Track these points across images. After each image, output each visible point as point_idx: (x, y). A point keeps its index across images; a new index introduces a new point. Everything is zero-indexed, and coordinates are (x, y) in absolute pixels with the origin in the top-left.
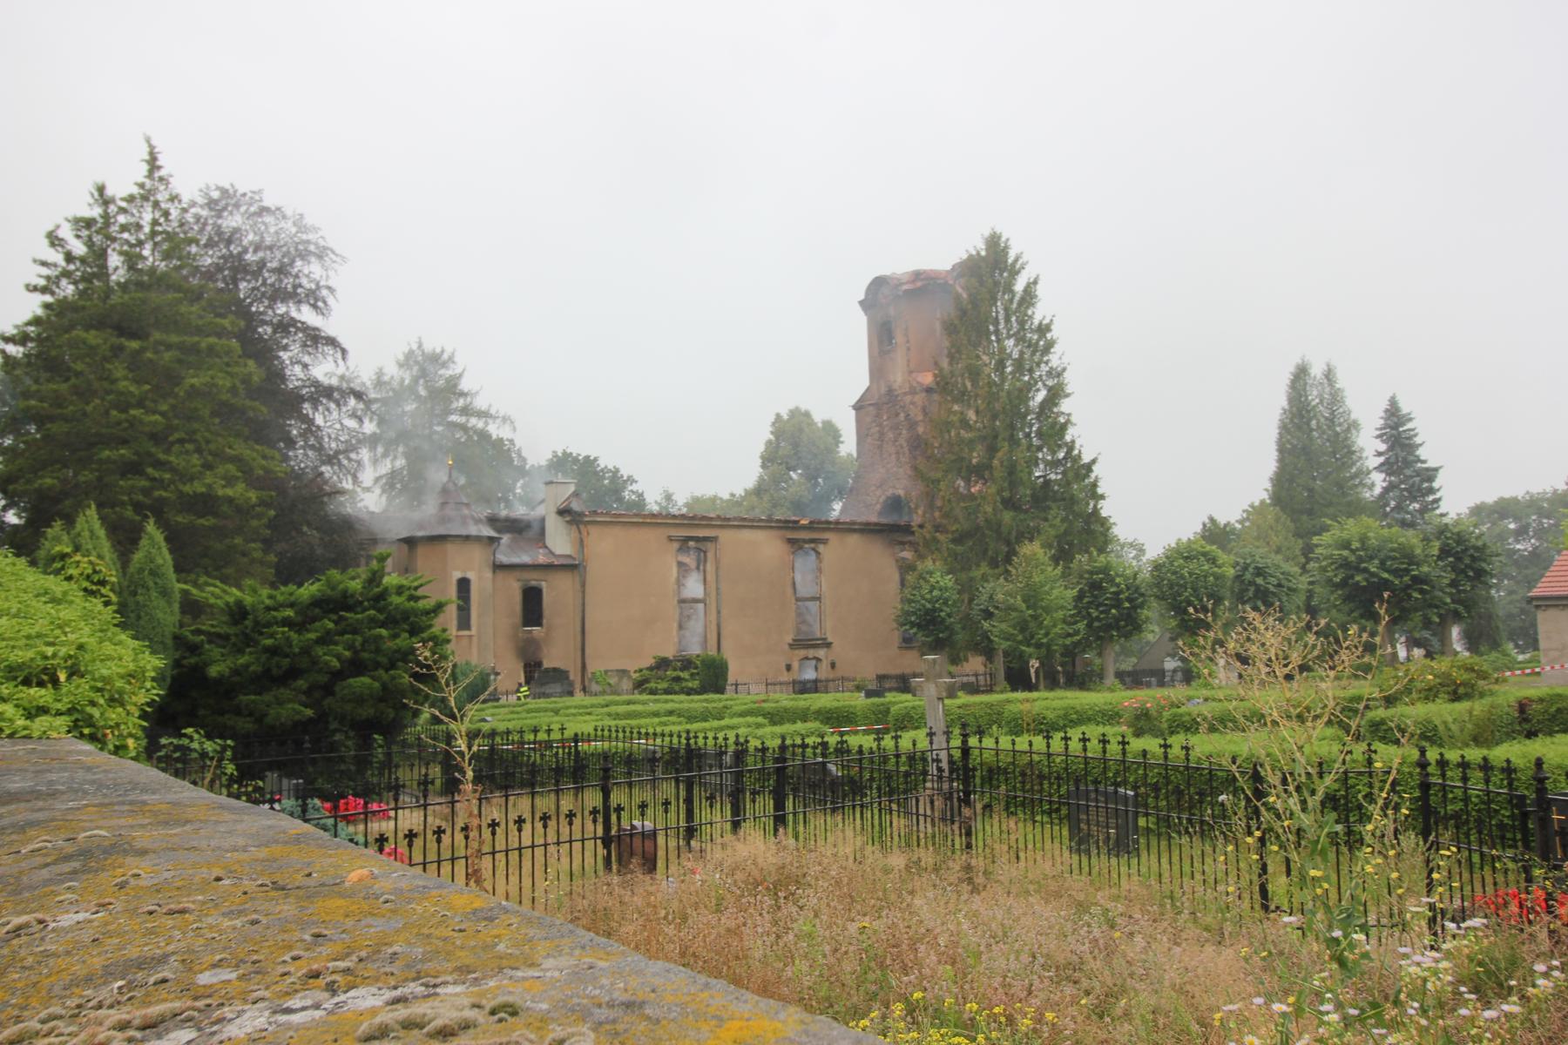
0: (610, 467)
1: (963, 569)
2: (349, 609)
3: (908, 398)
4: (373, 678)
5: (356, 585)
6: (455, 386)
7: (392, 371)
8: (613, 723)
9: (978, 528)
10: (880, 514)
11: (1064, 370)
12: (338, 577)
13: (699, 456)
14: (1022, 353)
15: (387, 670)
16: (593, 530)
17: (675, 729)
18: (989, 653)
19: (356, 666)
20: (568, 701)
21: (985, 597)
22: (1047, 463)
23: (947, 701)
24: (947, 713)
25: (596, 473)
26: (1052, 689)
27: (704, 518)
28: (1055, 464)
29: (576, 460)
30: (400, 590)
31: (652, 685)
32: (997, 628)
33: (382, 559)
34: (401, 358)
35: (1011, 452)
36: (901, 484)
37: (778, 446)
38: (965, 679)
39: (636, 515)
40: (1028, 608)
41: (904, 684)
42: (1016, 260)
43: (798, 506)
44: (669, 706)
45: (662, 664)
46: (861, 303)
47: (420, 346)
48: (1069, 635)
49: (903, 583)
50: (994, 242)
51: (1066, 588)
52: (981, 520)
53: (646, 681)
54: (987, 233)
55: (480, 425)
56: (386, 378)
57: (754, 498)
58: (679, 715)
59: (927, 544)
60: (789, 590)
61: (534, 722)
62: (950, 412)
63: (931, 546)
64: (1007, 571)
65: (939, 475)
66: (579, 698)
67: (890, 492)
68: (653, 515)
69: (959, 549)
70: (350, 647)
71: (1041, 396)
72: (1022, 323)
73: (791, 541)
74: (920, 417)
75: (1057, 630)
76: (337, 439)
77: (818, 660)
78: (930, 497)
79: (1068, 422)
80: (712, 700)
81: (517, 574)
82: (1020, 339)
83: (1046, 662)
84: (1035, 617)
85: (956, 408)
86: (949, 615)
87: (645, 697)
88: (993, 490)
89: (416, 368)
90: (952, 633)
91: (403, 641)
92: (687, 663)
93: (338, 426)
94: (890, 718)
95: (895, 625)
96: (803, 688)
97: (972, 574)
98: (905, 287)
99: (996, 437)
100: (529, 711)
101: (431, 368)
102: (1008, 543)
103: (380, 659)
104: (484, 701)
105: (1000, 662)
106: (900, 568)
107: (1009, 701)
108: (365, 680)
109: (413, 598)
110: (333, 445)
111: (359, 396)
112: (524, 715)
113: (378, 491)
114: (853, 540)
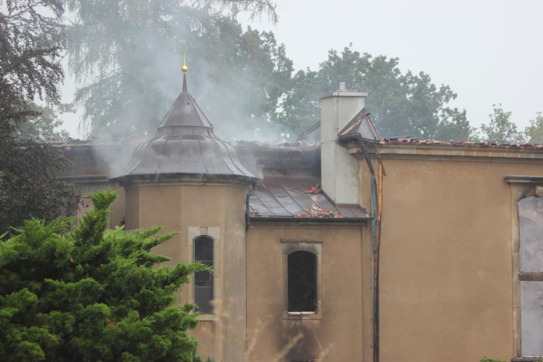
0: (416, 73)
2: (57, 274)
5: (66, 241)
25: (394, 83)
29: (364, 63)
30: (127, 248)
68: (483, 146)
70: (58, 329)
76: (26, 35)
81: (281, 232)
91: (133, 323)
93: (27, 16)
103: (99, 347)
109: (142, 260)
110: (22, 43)
113: (81, 110)
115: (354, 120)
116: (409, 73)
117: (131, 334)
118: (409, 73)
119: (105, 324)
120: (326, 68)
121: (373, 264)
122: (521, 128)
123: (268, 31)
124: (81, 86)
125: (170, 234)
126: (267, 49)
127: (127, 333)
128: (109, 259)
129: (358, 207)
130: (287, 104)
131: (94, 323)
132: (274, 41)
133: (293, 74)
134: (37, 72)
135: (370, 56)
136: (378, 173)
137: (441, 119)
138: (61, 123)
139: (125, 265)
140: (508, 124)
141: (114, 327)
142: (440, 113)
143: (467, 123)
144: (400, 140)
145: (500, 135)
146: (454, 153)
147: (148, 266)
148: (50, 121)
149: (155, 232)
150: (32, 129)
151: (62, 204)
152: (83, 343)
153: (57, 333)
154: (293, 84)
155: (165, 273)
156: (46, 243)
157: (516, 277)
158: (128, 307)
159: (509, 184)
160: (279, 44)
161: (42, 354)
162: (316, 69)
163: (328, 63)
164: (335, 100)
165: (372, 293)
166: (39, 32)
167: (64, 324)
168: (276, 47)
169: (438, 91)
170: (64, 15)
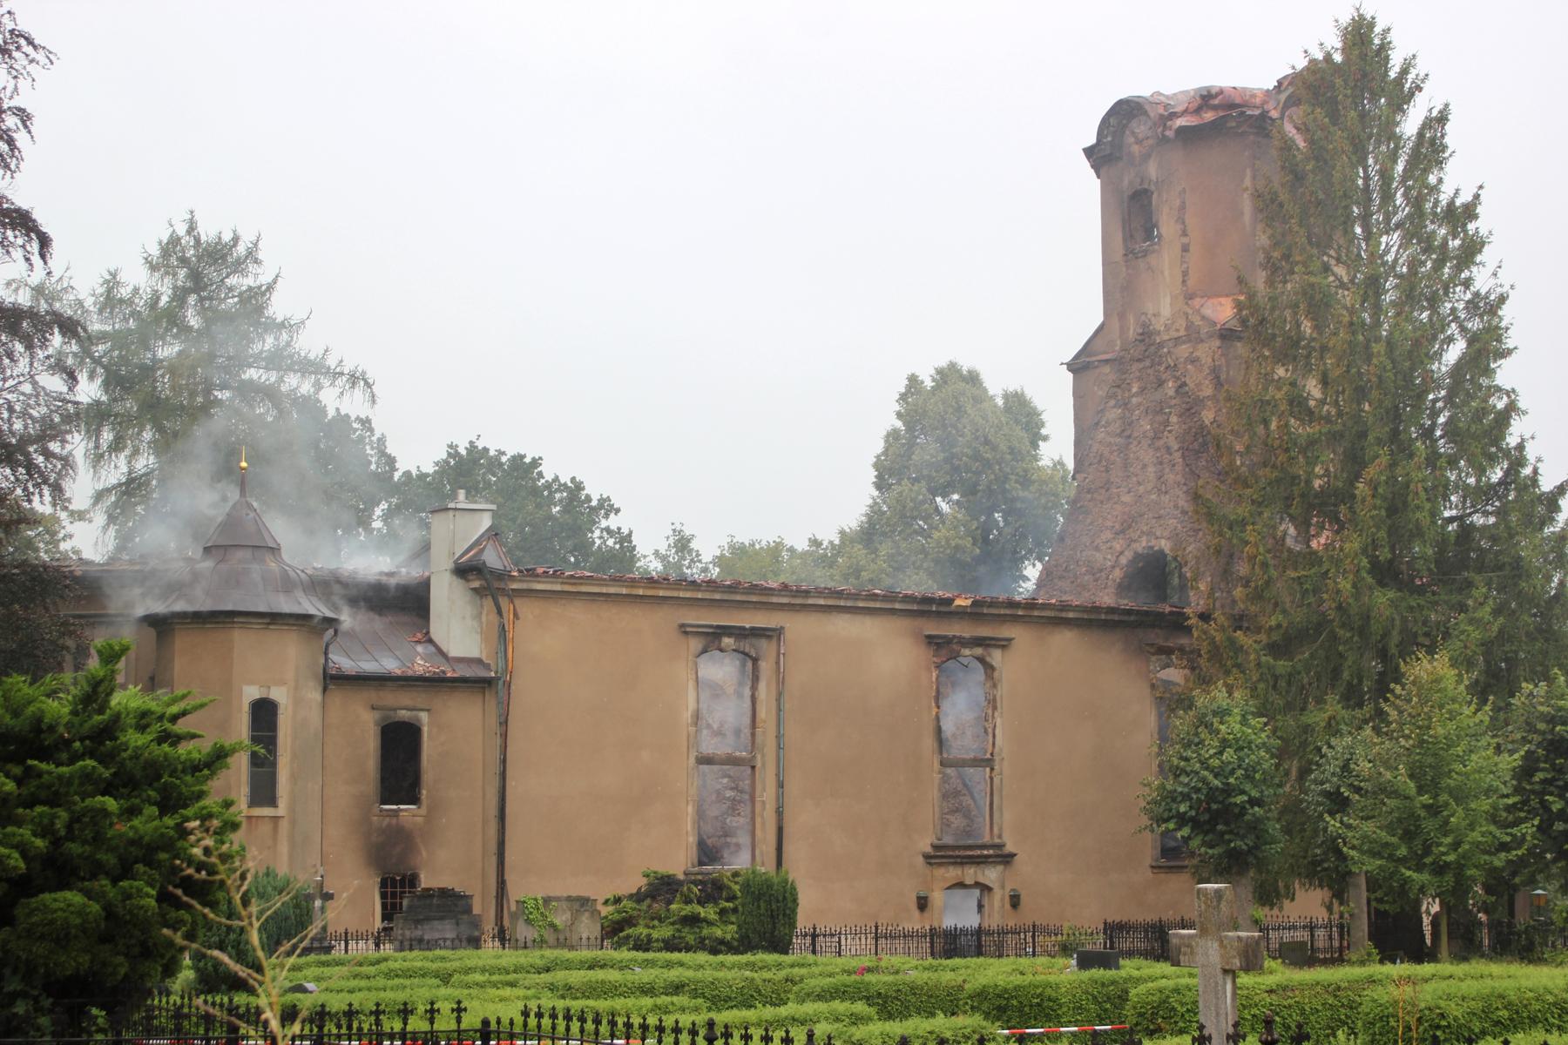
0: (565, 479)
1: (1289, 707)
2: (45, 754)
3: (1183, 350)
4: (88, 894)
5: (58, 708)
6: (260, 309)
7: (137, 279)
8: (561, 1005)
9: (1322, 624)
10: (1123, 588)
11: (1502, 299)
12: (27, 690)
13: (745, 460)
14: (1414, 264)
15: (115, 881)
16: (528, 609)
17: (686, 1020)
18: (1338, 883)
19: (57, 870)
20: (469, 957)
21: (1333, 767)
22: (1467, 492)
23: (1245, 979)
24: (1244, 1002)
25: (535, 492)
26: (1465, 959)
27: (753, 589)
28: (1485, 493)
29: (494, 463)
30: (143, 720)
31: (641, 931)
32: (1356, 831)
33: (111, 656)
34: (155, 251)
35: (1393, 465)
36: (1166, 528)
37: (911, 444)
38: (1287, 936)
39: (615, 580)
40: (1421, 790)
41: (1158, 942)
42: (1404, 71)
44: (674, 974)
45: (662, 888)
46: (1089, 152)
47: (192, 228)
48: (1504, 847)
49: (1163, 738)
50: (1360, 35)
51: (1498, 749)
53: (629, 922)
54: (1345, 19)
55: (306, 388)
56: (124, 292)
57: (859, 551)
58: (695, 994)
59: (1215, 654)
60: (929, 742)
61: (401, 996)
62: (1268, 379)
63: (1224, 659)
64: (1380, 714)
65: (1243, 510)
66: (491, 953)
67: (1141, 546)
68: (651, 582)
69: (1282, 666)
70: (45, 831)
71: (1454, 353)
72: (1417, 203)
73: (931, 640)
74: (1208, 391)
75: (1475, 836)
76: (25, 414)
77: (985, 889)
78: (1225, 556)
79: (1512, 407)
80: (764, 966)
81: (372, 695)
82: (1414, 230)
83: (1454, 899)
84: (1433, 810)
85: (1281, 372)
87: (625, 954)
88: (1354, 544)
89: (182, 273)
91: (148, 823)
92: (713, 890)
93: (27, 388)
94: (1128, 1011)
95: (1145, 821)
96: (950, 944)
98: (1180, 122)
99: (1363, 435)
100: (390, 975)
101: (211, 273)
102: (1383, 655)
103: (102, 856)
104: (307, 951)
105: (1359, 898)
107: (1372, 981)
108: (74, 897)
109: (165, 737)
110: (18, 426)
111: (70, 327)
112: (381, 982)
113: (100, 518)
114: (1065, 641)
115: (477, 542)
116: (556, 479)
117: (147, 839)
118: (556, 479)
119: (111, 825)
120: (444, 468)
121: (499, 741)
122: (707, 557)
123: (363, 416)
124: (100, 486)
125: (205, 700)
126: (361, 439)
127: (141, 838)
128: (118, 734)
129: (479, 661)
130: (386, 517)
131: (95, 824)
132: (371, 430)
133: (397, 476)
134: (37, 466)
135: (504, 453)
136: (509, 616)
137: (598, 542)
138: (71, 536)
139: (139, 743)
140: (690, 551)
141: (124, 829)
142: (597, 533)
143: (634, 548)
144: (540, 571)
145: (678, 566)
146: (612, 590)
147: (171, 745)
148: (55, 533)
149: (184, 697)
150: (30, 544)
151: (67, 648)
152: (80, 850)
153: (43, 836)
154: (396, 489)
155: (196, 755)
156: (31, 709)
157: (692, 760)
158: (143, 801)
159: (686, 633)
160: (377, 435)
161: (22, 865)
162: (429, 468)
163: (446, 462)
164: (451, 513)
165: (496, 782)
166: (44, 410)
167: (53, 824)
168: (374, 439)
169: (594, 503)
170: (78, 388)
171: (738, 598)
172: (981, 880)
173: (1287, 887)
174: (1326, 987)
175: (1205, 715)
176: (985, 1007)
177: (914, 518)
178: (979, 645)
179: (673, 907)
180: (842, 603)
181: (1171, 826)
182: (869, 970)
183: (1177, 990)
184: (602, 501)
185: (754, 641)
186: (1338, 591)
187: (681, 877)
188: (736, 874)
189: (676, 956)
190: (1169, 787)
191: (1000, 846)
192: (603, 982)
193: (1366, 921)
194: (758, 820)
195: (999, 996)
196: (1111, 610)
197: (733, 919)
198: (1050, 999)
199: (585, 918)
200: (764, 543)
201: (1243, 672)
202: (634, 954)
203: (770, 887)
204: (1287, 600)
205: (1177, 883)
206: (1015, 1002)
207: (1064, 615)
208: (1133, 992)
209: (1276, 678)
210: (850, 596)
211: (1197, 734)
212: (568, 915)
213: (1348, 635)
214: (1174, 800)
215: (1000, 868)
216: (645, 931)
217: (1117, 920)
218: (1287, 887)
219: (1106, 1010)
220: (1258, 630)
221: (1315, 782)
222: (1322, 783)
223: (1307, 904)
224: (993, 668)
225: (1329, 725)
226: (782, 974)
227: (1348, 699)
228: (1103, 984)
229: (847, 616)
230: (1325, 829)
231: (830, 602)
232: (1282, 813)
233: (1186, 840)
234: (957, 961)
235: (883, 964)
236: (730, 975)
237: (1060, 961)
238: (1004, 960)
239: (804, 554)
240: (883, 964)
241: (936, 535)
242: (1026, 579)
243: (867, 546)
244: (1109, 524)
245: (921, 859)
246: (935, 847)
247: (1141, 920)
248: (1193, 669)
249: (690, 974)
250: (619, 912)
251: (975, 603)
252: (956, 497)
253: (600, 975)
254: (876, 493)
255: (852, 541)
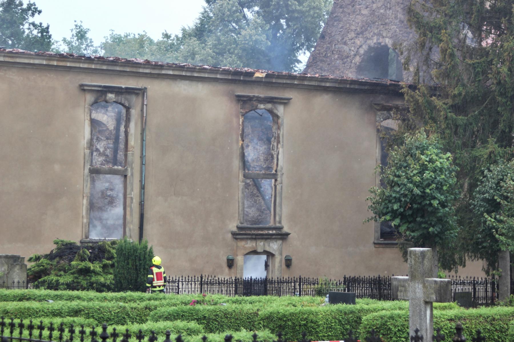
1: (465, 145)
9: (487, 93)
10: (360, 69)
18: (492, 256)
21: (491, 183)
27: (128, 63)
31: (53, 278)
38: (459, 288)
41: (382, 289)
43: (252, 53)
44: (74, 304)
45: (66, 251)
49: (384, 158)
52: (491, 83)
53: (45, 272)
59: (418, 110)
60: (236, 163)
67: (373, 42)
68: (61, 57)
69: (461, 119)
73: (243, 101)
77: (270, 255)
80: (134, 299)
86: (443, 205)
87: (43, 292)
90: (446, 228)
92: (99, 251)
94: (361, 330)
96: (249, 288)
97: (476, 153)
106: (382, 140)
114: (323, 101)
137: (27, 32)
142: (26, 26)
143: (50, 37)
145: (78, 48)
146: (37, 62)
157: (87, 171)
171: (118, 68)
172: (268, 249)
173: (461, 258)
174: (486, 319)
175: (411, 149)
176: (271, 325)
177: (230, 22)
178: (269, 102)
179: (73, 263)
180: (184, 74)
181: (388, 217)
182: (198, 302)
183: (392, 318)
184: (30, 6)
185: (128, 97)
186: (499, 73)
187: (79, 244)
188: (114, 243)
189: (75, 293)
190: (387, 194)
191: (281, 228)
192: (29, 309)
193: (509, 280)
194: (128, 209)
195: (280, 319)
196: (353, 82)
197: (111, 271)
198: (312, 322)
199: (17, 269)
200: (132, 36)
201: (435, 122)
202: (48, 292)
203: (135, 250)
204: (465, 78)
205: (390, 256)
206: (290, 323)
207: (323, 84)
208: (364, 318)
209: (457, 126)
210: (189, 69)
211: (405, 161)
212: (6, 267)
213: (504, 100)
214: (390, 202)
215: (280, 242)
216: (55, 278)
217: (352, 276)
218: (461, 258)
219: (347, 329)
220: (447, 96)
221: (479, 192)
222: (484, 193)
223: (474, 269)
224: (278, 117)
225: (490, 157)
226: (143, 304)
227: (502, 141)
228: (345, 313)
229: (187, 82)
230: (485, 222)
231: (177, 73)
232: (458, 211)
233: (397, 227)
234: (254, 298)
235: (207, 298)
236: (110, 304)
237: (318, 299)
238: (283, 298)
239: (159, 44)
240: (207, 298)
241: (243, 32)
242: (299, 62)
243: (199, 39)
244: (353, 28)
245: (230, 235)
246: (239, 228)
247: (367, 276)
248: (404, 120)
249: (85, 303)
250: (38, 266)
251: (268, 76)
252: (256, 9)
253: (26, 304)
254: (206, 5)
255: (190, 35)
